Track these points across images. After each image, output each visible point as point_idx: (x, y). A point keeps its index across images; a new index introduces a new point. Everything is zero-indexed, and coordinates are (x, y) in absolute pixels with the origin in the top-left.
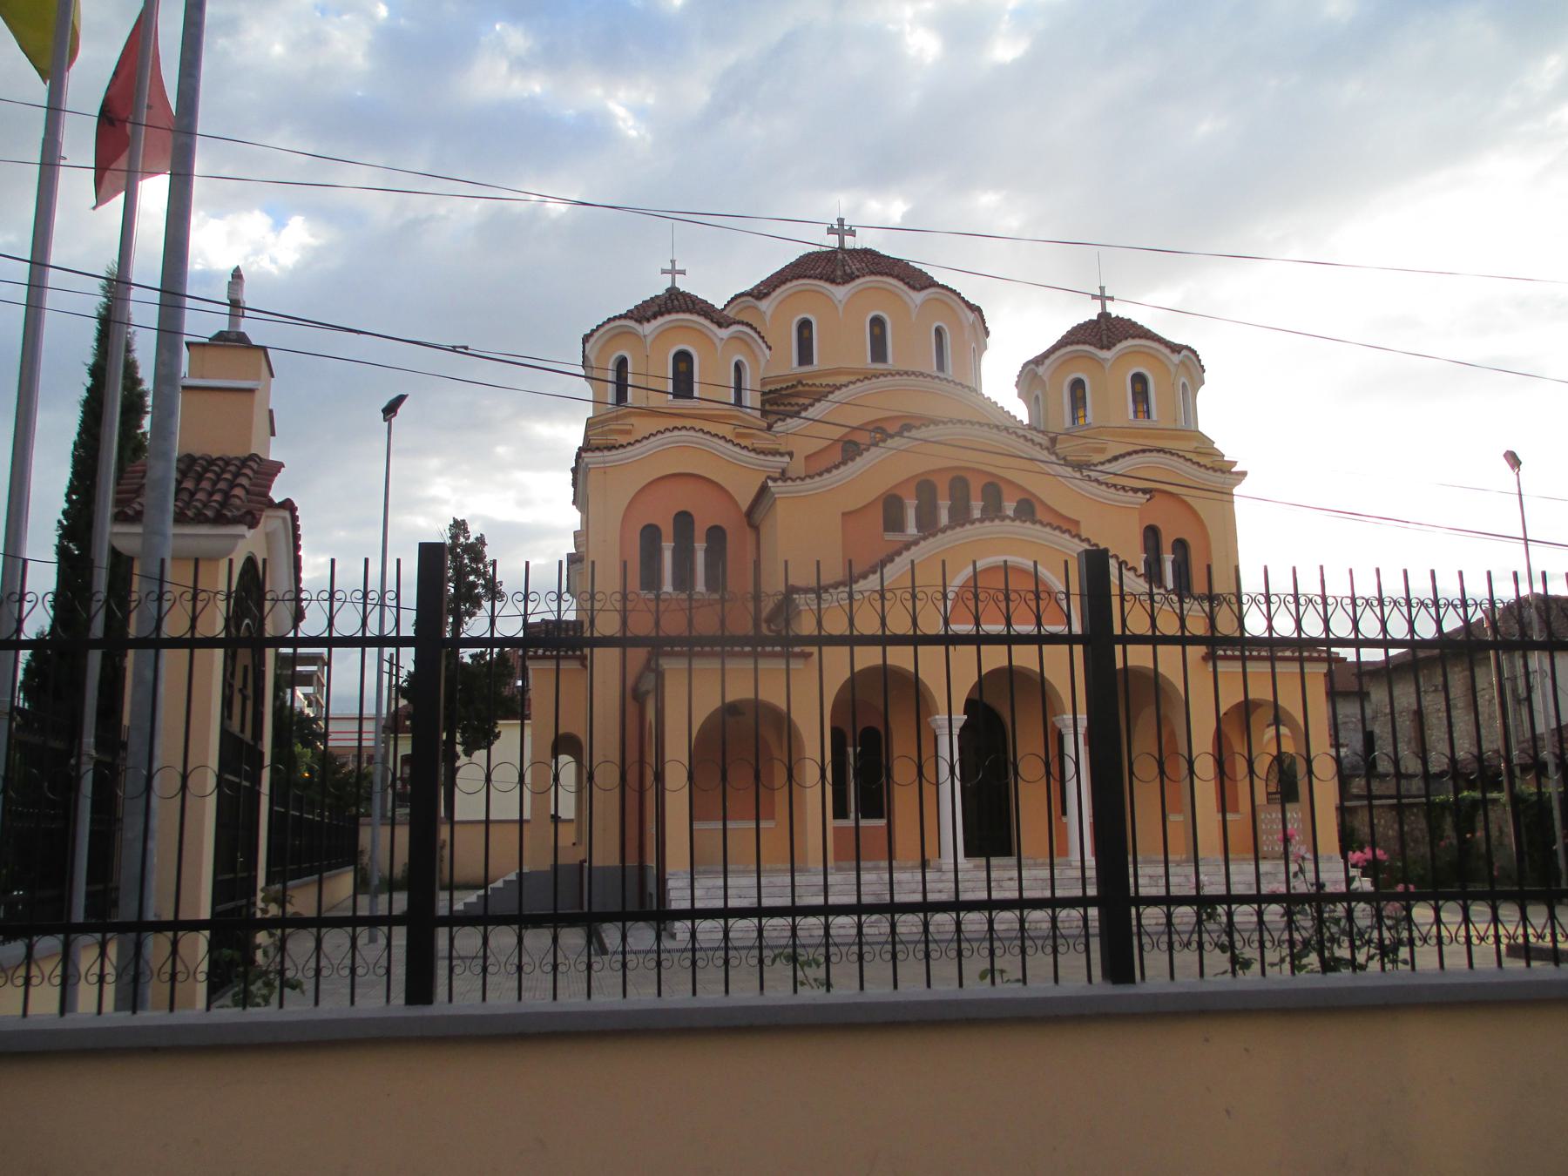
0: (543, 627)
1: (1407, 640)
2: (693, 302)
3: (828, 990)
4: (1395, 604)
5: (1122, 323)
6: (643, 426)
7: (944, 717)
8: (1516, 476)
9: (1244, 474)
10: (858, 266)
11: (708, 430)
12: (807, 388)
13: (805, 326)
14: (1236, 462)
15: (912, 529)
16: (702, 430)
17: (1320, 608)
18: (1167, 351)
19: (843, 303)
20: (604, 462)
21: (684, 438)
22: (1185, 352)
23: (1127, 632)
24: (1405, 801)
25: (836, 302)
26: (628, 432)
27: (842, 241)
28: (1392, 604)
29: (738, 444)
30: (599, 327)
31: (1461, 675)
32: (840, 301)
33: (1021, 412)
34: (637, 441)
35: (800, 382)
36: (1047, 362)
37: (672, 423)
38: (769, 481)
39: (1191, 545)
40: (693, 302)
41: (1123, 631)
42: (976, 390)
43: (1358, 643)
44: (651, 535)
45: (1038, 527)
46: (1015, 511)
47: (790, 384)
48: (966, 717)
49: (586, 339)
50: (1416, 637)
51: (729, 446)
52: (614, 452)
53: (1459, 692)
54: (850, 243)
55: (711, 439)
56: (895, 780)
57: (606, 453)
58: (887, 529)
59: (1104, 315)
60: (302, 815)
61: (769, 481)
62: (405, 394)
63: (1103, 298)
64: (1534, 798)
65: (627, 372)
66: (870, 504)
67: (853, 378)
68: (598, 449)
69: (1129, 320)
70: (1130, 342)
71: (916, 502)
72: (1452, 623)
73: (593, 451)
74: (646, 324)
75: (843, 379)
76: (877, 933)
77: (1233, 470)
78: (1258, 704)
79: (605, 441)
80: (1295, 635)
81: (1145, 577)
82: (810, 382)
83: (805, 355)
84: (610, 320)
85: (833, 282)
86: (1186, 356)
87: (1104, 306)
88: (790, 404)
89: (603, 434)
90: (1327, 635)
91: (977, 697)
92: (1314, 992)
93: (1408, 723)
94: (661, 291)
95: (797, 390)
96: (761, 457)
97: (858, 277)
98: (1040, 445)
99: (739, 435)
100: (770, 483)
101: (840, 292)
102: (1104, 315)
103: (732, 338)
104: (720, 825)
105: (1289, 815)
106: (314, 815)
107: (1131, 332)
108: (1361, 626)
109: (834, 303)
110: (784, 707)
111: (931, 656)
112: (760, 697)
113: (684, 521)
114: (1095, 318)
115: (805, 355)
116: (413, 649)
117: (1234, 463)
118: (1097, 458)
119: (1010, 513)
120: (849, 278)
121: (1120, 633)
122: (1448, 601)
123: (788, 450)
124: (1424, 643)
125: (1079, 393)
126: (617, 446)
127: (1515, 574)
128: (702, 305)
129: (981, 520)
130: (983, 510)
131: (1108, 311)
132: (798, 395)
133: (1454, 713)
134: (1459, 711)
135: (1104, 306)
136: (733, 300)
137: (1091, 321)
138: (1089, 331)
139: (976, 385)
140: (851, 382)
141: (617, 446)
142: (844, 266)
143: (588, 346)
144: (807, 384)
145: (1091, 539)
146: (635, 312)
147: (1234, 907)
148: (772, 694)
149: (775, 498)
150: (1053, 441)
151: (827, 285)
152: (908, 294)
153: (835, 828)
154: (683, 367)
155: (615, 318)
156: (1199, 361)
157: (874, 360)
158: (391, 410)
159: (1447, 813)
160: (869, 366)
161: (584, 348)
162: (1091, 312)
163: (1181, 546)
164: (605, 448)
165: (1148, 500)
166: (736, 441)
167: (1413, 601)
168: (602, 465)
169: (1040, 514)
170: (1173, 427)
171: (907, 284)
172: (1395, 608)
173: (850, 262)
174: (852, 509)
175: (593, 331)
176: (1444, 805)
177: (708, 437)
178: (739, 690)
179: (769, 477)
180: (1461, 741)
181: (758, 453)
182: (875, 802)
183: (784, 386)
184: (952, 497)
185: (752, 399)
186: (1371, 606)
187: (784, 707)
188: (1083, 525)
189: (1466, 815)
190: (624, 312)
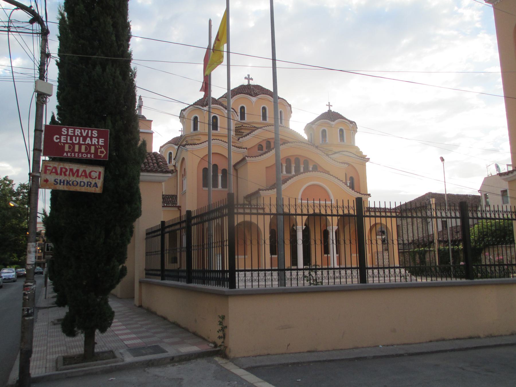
3: (219, 316)
7: (300, 226)
8: (443, 164)
10: (258, 91)
11: (221, 139)
12: (244, 128)
15: (293, 173)
16: (221, 140)
19: (255, 102)
20: (193, 149)
24: (405, 251)
25: (253, 102)
26: (199, 140)
32: (254, 102)
33: (306, 137)
35: (242, 126)
42: (290, 129)
44: (205, 170)
45: (319, 173)
47: (239, 126)
52: (196, 146)
54: (252, 83)
55: (219, 141)
56: (260, 244)
57: (193, 146)
59: (330, 111)
63: (329, 106)
64: (443, 250)
65: (198, 121)
66: (273, 165)
67: (264, 126)
69: (337, 113)
70: (339, 120)
71: (295, 165)
73: (189, 145)
77: (366, 157)
78: (378, 224)
81: (349, 187)
85: (251, 95)
87: (329, 108)
88: (240, 132)
89: (191, 140)
92: (459, 282)
96: (238, 149)
97: (259, 95)
100: (246, 158)
101: (254, 99)
102: (330, 111)
104: (244, 257)
105: (384, 254)
109: (252, 102)
110: (256, 223)
112: (252, 221)
114: (327, 111)
117: (366, 156)
120: (256, 95)
125: (243, 110)
129: (312, 171)
131: (250, 83)
132: (242, 129)
133: (408, 226)
134: (410, 225)
135: (329, 108)
142: (253, 91)
144: (244, 126)
149: (247, 162)
157: (263, 120)
159: (417, 254)
160: (261, 122)
165: (348, 166)
173: (255, 89)
176: (416, 252)
177: (223, 142)
181: (237, 148)
184: (295, 163)
187: (256, 223)
189: (423, 255)
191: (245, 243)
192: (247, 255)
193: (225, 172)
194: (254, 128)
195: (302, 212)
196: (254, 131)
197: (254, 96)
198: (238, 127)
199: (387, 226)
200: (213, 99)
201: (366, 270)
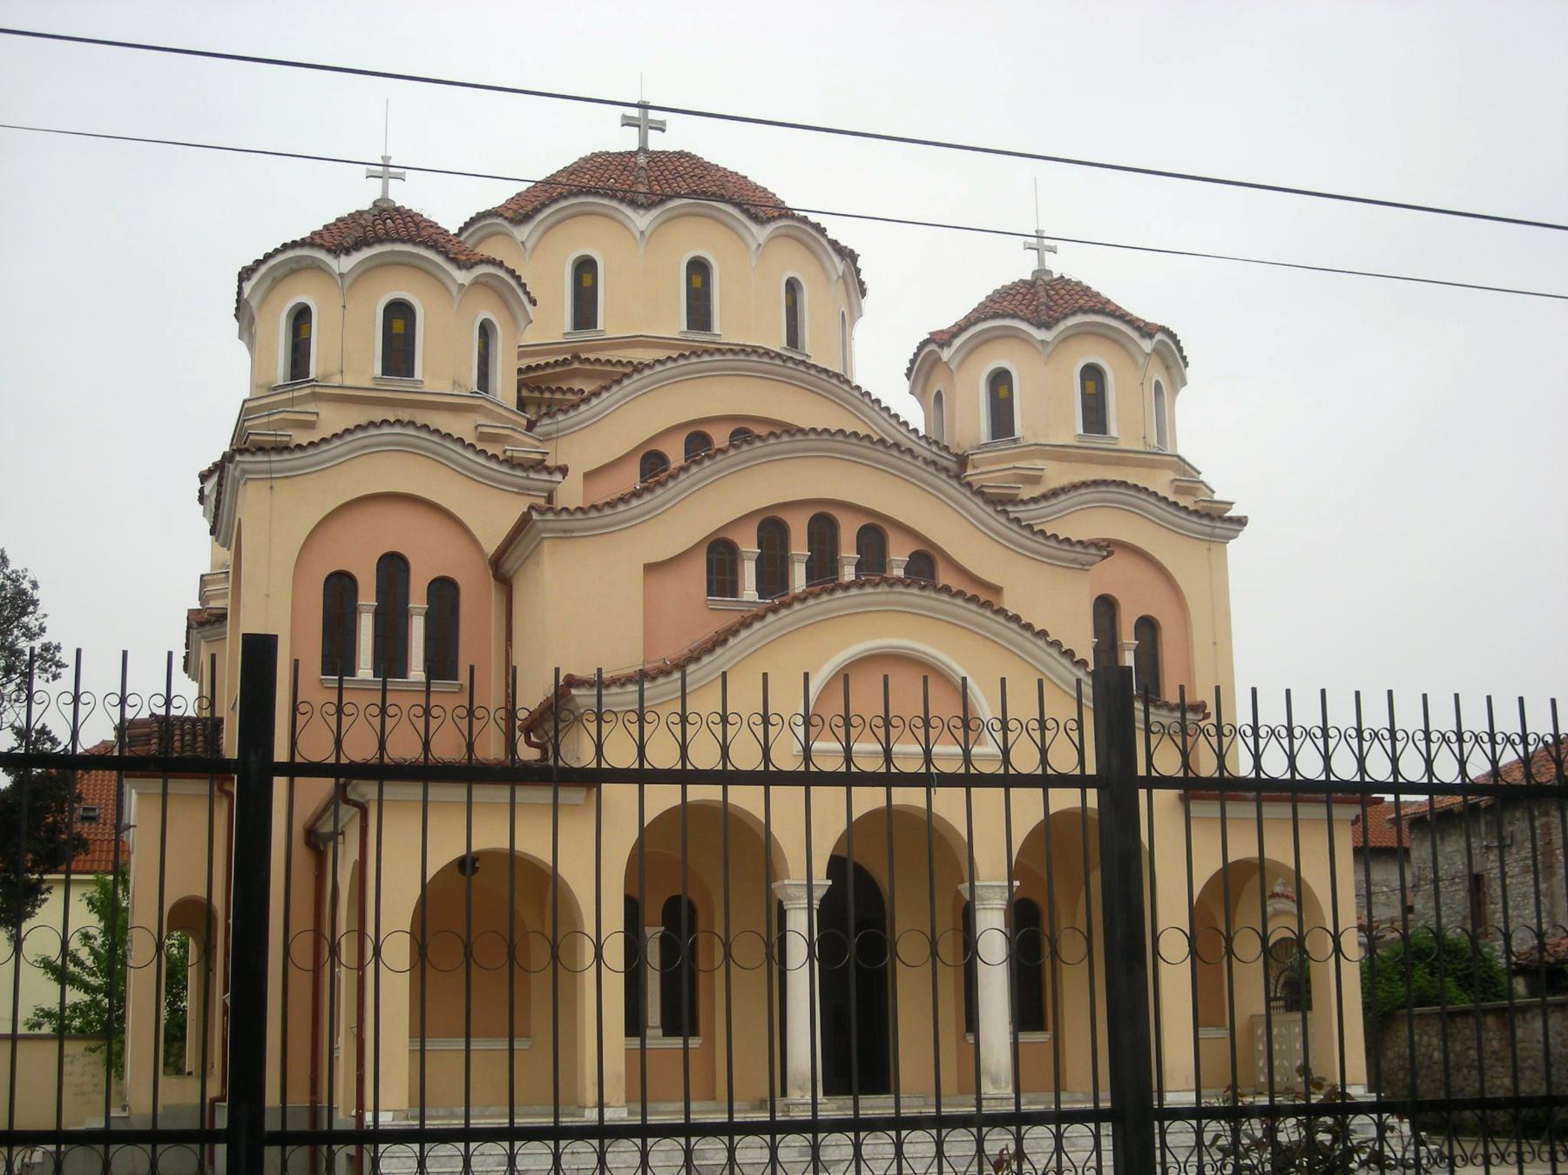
0: (155, 727)
1: (1215, 778)
2: (416, 224)
4: (1477, 741)
5: (1069, 287)
6: (333, 419)
9: (1241, 522)
13: (585, 267)
14: (1232, 504)
17: (1388, 744)
18: (1135, 335)
21: (374, 440)
22: (1159, 336)
23: (1154, 774)
27: (644, 139)
28: (1505, 739)
29: (483, 452)
30: (268, 257)
32: (642, 233)
34: (324, 440)
35: (576, 357)
36: (957, 342)
37: (378, 414)
39: (1148, 614)
40: (416, 224)
41: (1149, 771)
43: (1398, 787)
44: (340, 587)
46: (908, 570)
47: (561, 358)
49: (245, 275)
50: (1401, 780)
51: (470, 455)
52: (286, 456)
54: (657, 142)
58: (708, 596)
59: (1041, 272)
67: (662, 354)
68: (261, 449)
69: (1079, 284)
72: (1478, 767)
74: (343, 258)
75: (646, 355)
77: (1229, 514)
79: (273, 439)
80: (1358, 779)
82: (592, 357)
83: (585, 310)
84: (285, 247)
85: (633, 204)
86: (1160, 342)
87: (1041, 260)
90: (1396, 778)
91: (844, 854)
93: (1463, 894)
94: (366, 205)
95: (573, 367)
98: (946, 470)
99: (484, 437)
100: (535, 516)
103: (476, 282)
107: (1082, 302)
108: (1436, 767)
111: (787, 799)
113: (393, 568)
114: (1028, 277)
116: (275, 778)
119: (899, 572)
121: (1145, 774)
122: (1538, 736)
123: (559, 464)
124: (1446, 789)
125: (399, 326)
126: (292, 446)
127: (170, 654)
128: (432, 230)
129: (858, 584)
130: (859, 567)
132: (575, 374)
135: (1041, 260)
136: (473, 221)
137: (1023, 282)
138: (1019, 297)
139: (845, 371)
140: (658, 361)
141: (292, 446)
143: (247, 287)
144: (587, 360)
146: (326, 236)
147: (904, 1133)
148: (533, 843)
150: (963, 461)
151: (624, 208)
152: (748, 228)
154: (399, 326)
155: (294, 245)
156: (1180, 350)
161: (240, 287)
162: (1021, 267)
164: (273, 449)
166: (479, 446)
167: (1295, 731)
168: (273, 476)
169: (944, 577)
171: (746, 212)
172: (1477, 744)
174: (659, 559)
175: (258, 263)
178: (490, 836)
179: (531, 507)
182: (680, 1019)
183: (552, 360)
185: (505, 386)
186: (1448, 742)
188: (1006, 594)
190: (306, 234)
191: (555, 957)
192: (527, 1035)
193: (444, 592)
194: (619, 369)
195: (1044, 761)
196: (619, 382)
197: (641, 206)
198: (547, 364)
199: (1303, 874)
200: (454, 234)
201: (1156, 1123)
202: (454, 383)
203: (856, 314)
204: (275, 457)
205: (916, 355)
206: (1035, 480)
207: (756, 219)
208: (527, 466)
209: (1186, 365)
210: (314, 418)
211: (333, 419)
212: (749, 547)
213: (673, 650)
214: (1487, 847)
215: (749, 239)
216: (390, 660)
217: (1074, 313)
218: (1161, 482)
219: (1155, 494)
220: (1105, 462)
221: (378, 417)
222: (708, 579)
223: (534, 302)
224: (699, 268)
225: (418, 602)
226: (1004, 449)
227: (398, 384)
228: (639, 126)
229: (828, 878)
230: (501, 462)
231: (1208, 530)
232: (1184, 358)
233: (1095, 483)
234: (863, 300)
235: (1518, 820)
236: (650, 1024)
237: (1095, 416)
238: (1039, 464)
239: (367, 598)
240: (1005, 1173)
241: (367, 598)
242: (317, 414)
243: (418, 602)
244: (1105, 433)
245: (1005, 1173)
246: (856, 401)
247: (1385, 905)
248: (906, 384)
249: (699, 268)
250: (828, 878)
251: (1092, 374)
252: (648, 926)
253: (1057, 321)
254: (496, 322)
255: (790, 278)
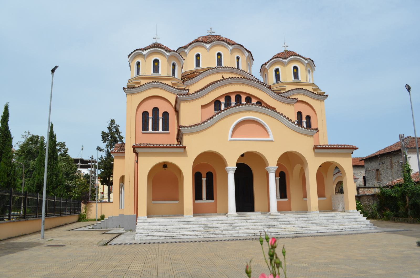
6: (143, 82)
9: (327, 96)
13: (198, 56)
18: (304, 60)
30: (132, 53)
31: (389, 159)
32: (208, 48)
38: (178, 95)
39: (309, 115)
44: (145, 114)
48: (236, 167)
53: (389, 164)
60: (55, 200)
61: (178, 95)
62: (58, 65)
76: (203, 237)
83: (198, 64)
84: (135, 51)
85: (206, 43)
86: (309, 61)
93: (375, 173)
106: (54, 199)
113: (156, 110)
115: (198, 64)
118: (282, 92)
134: (389, 169)
145: (243, 70)
151: (204, 44)
153: (208, 199)
156: (314, 63)
158: (53, 71)
163: (308, 118)
170: (306, 82)
180: (389, 178)
185: (178, 75)
193: (166, 114)
197: (207, 43)
202: (167, 74)
203: (252, 64)
204: (131, 90)
205: (261, 68)
206: (139, 83)
207: (230, 44)
208: (181, 89)
209: (315, 67)
210: (139, 82)
211: (143, 82)
212: (223, 101)
213: (203, 121)
214: (379, 164)
215: (229, 48)
216: (155, 128)
217: (291, 56)
218: (310, 88)
219: (309, 91)
220: (297, 85)
221: (151, 81)
222: (215, 108)
223: (184, 60)
224: (219, 54)
225: (161, 116)
226: (279, 85)
227: (156, 75)
228: (210, 32)
229: (236, 166)
230: (176, 89)
231: (320, 98)
232: (315, 65)
233: (296, 89)
234: (253, 62)
235: (385, 159)
236: (204, 198)
237: (296, 75)
238: (285, 86)
239: (151, 116)
240: (132, 276)
241: (151, 116)
242: (140, 81)
243: (161, 116)
244: (298, 79)
245: (132, 276)
246: (284, 121)
247: (360, 176)
248: (260, 74)
249: (219, 54)
250: (236, 166)
251: (295, 68)
252: (204, 178)
253: (288, 58)
254: (176, 63)
255: (238, 56)
